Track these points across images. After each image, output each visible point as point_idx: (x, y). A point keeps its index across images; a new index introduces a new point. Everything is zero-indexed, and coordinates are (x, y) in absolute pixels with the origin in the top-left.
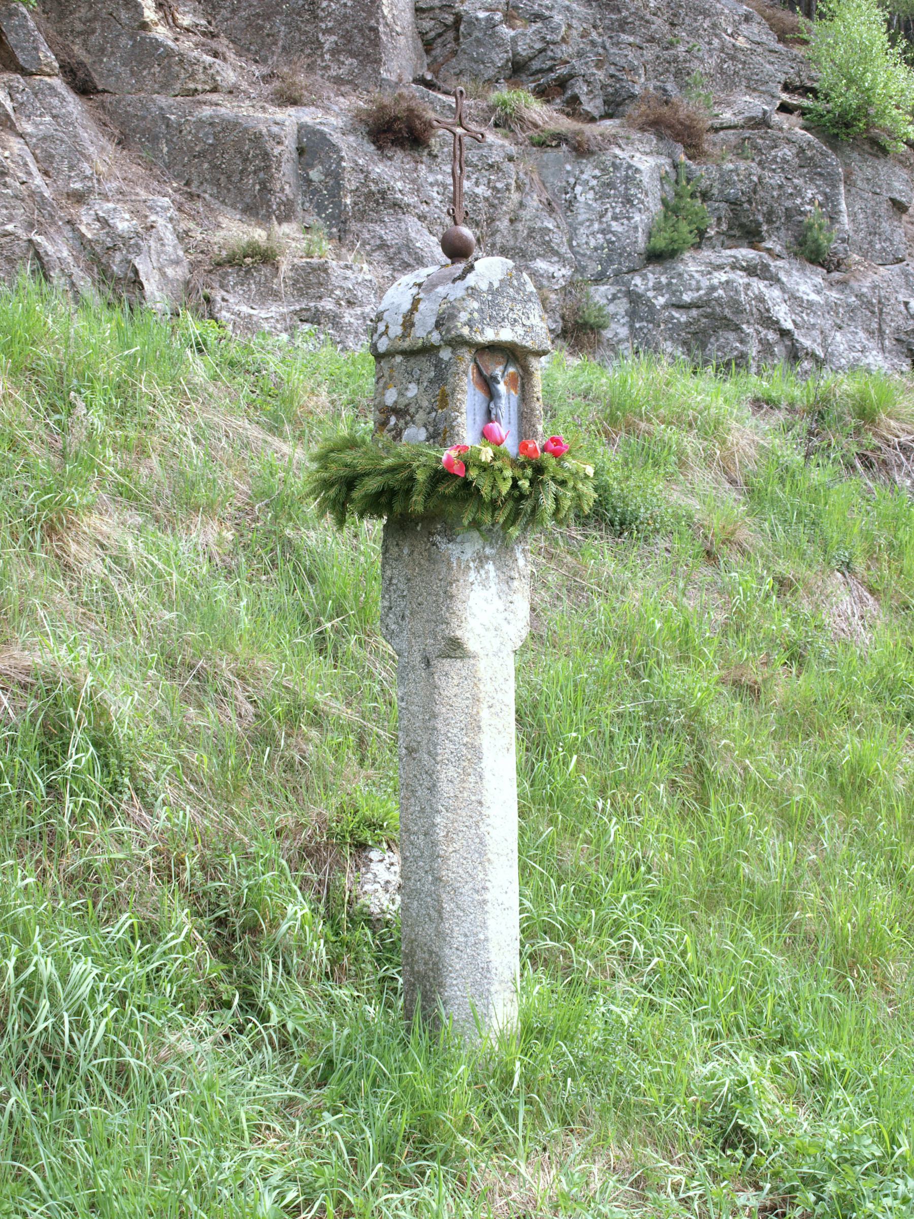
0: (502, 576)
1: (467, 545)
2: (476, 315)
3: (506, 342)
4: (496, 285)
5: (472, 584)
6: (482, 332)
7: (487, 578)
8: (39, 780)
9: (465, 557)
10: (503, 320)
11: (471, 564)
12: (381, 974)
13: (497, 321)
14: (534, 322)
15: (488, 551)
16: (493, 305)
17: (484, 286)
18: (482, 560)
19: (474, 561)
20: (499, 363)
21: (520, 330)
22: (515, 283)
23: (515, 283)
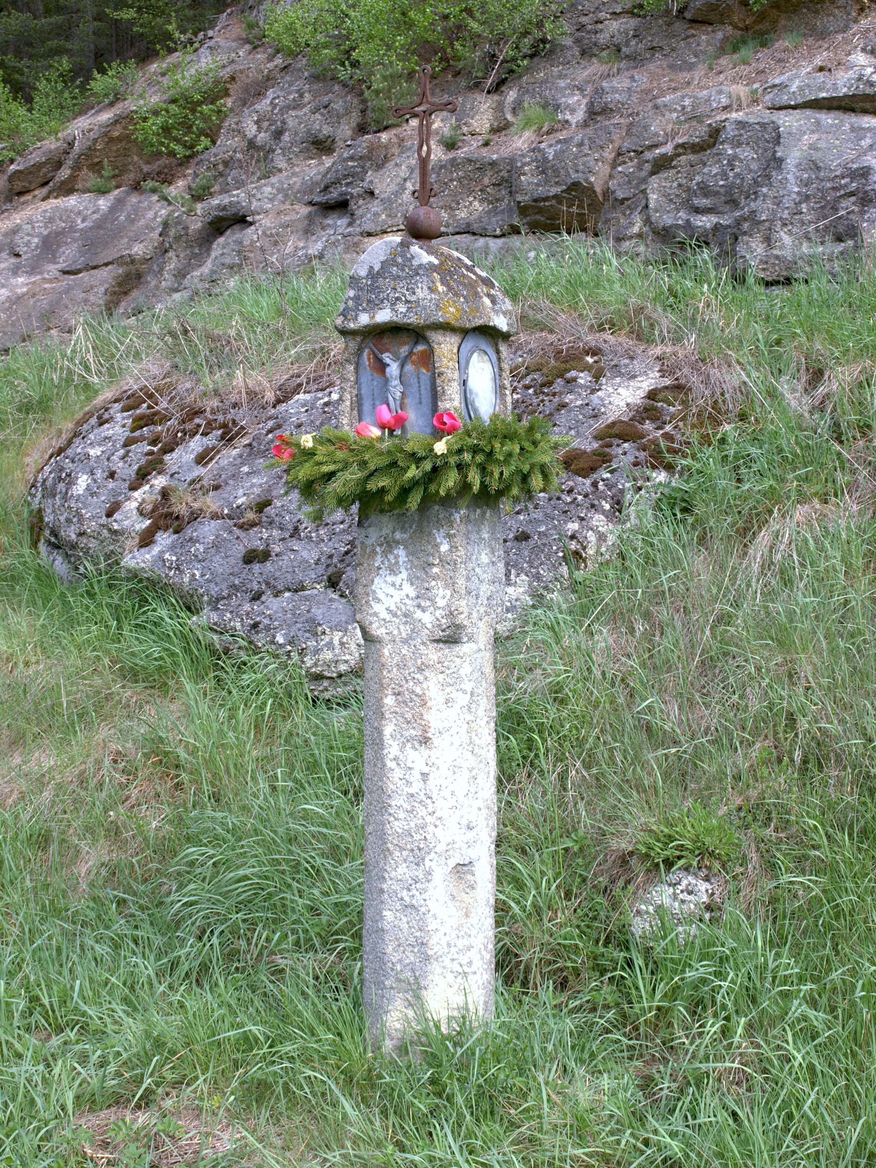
0: (416, 562)
1: (371, 529)
2: (350, 303)
3: (386, 323)
4: (377, 267)
5: (379, 568)
6: (356, 319)
7: (397, 563)
8: (241, 872)
9: (369, 542)
10: (382, 302)
11: (378, 549)
12: (97, 803)
13: (374, 306)
14: (421, 296)
15: (398, 536)
16: (373, 289)
17: (363, 273)
18: (390, 545)
19: (381, 545)
20: (405, 344)
21: (402, 308)
22: (400, 260)
23: (400, 260)
